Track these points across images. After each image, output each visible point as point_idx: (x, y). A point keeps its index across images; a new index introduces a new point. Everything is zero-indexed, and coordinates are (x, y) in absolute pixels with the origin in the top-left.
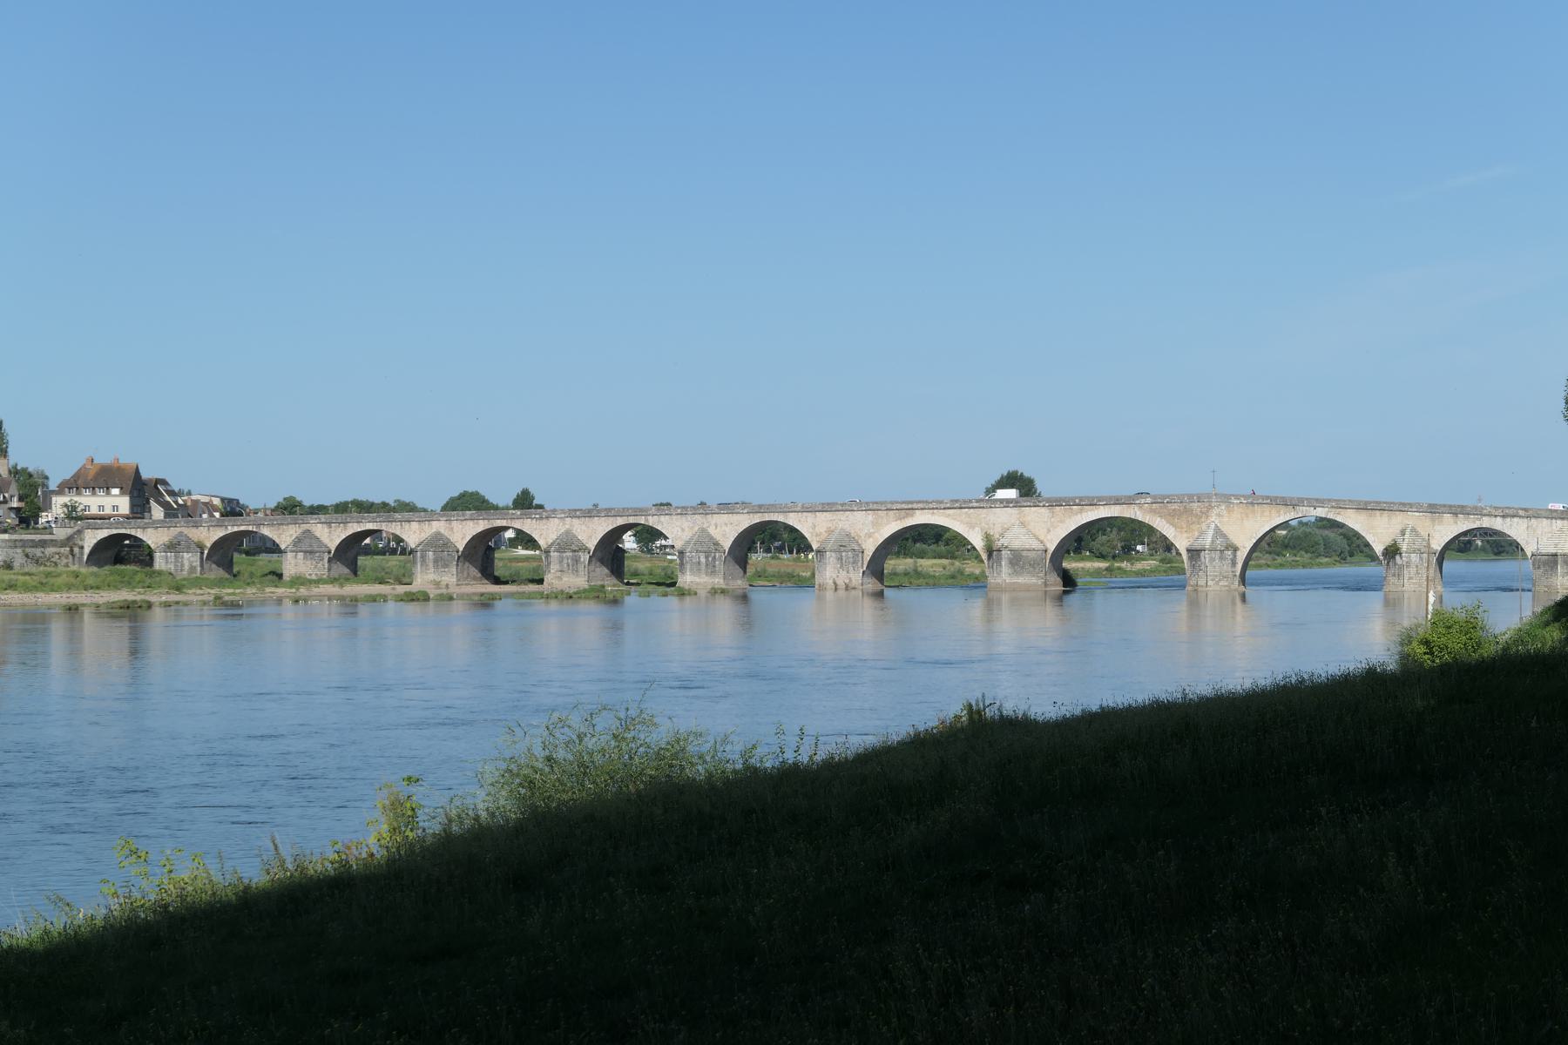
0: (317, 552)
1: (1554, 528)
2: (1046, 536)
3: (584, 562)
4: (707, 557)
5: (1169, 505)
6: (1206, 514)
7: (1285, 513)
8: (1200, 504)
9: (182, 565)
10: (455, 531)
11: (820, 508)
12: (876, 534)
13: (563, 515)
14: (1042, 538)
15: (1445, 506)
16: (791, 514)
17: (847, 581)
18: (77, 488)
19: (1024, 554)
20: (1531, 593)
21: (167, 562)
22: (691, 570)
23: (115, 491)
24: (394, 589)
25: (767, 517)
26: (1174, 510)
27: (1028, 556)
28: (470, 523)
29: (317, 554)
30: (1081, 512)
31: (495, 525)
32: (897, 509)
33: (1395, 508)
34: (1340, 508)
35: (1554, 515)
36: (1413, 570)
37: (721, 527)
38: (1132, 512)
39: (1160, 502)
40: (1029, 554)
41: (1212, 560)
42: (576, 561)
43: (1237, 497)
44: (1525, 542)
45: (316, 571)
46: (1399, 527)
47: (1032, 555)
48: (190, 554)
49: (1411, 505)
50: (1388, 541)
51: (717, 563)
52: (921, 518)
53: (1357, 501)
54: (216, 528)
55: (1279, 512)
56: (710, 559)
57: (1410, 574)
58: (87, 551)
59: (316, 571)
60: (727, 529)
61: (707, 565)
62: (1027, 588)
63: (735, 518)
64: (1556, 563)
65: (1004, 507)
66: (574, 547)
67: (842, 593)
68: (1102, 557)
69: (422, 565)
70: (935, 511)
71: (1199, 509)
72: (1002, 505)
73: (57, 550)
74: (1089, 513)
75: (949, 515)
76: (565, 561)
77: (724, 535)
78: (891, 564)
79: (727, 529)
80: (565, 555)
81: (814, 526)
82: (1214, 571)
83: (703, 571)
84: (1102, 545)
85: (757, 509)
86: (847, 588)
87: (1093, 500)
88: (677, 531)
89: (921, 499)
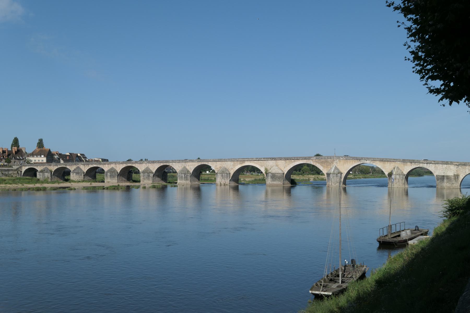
1: (444, 167)
4: (185, 175)
5: (321, 160)
6: (332, 162)
11: (218, 161)
15: (408, 160)
16: (210, 162)
17: (225, 183)
19: (276, 175)
29: (80, 174)
30: (294, 162)
36: (397, 180)
40: (278, 175)
42: (149, 176)
51: (188, 177)
54: (55, 166)
55: (355, 162)
56: (186, 176)
61: (185, 177)
62: (277, 186)
65: (271, 160)
69: (106, 177)
70: (251, 161)
73: (13, 172)
86: (224, 185)
87: (298, 158)
89: (245, 158)
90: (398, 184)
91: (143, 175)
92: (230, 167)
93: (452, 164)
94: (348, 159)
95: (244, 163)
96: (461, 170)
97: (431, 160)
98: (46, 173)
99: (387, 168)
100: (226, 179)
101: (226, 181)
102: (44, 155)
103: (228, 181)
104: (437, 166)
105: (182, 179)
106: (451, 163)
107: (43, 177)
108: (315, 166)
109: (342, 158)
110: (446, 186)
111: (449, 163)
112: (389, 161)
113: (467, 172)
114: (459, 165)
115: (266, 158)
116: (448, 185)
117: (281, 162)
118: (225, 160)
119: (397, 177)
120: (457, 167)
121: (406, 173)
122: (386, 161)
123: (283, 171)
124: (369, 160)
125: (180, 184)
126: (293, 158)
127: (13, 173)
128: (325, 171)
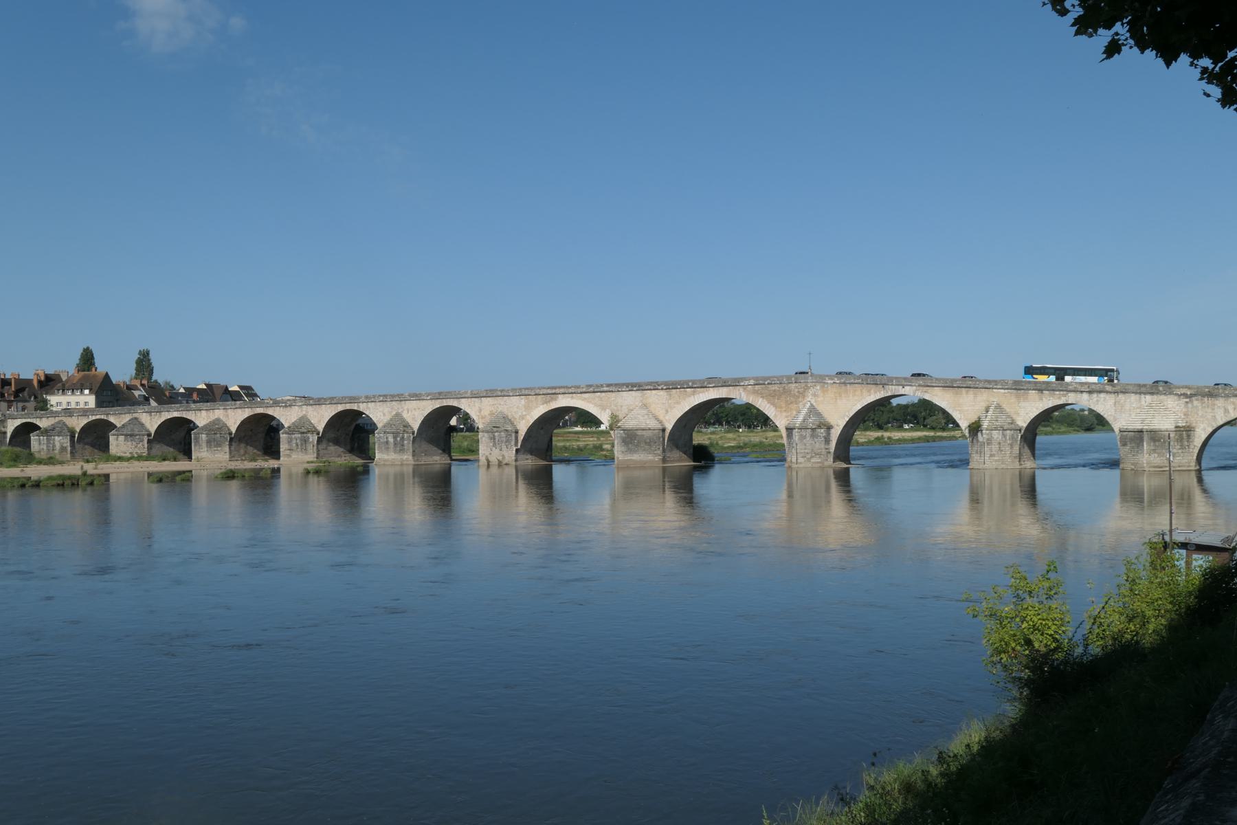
0: (137, 435)
1: (1143, 403)
2: (664, 416)
3: (313, 441)
4: (395, 438)
5: (770, 386)
6: (803, 394)
8: (797, 385)
9: (54, 446)
10: (230, 417)
11: (484, 395)
12: (528, 416)
13: (300, 404)
14: (661, 418)
16: (463, 400)
17: (500, 458)
18: (63, 390)
19: (639, 433)
20: (1116, 473)
21: (40, 444)
22: (380, 448)
23: (87, 392)
24: (96, 468)
25: (348, 407)
26: (774, 391)
27: (643, 435)
28: (239, 411)
29: (138, 437)
30: (694, 393)
31: (256, 412)
32: (543, 394)
33: (981, 385)
34: (928, 386)
35: (1143, 389)
36: (995, 447)
37: (412, 411)
39: (761, 382)
40: (644, 433)
41: (802, 438)
42: (305, 441)
43: (831, 377)
44: (1112, 418)
46: (984, 405)
47: (648, 434)
48: (61, 438)
49: (996, 382)
50: (973, 418)
52: (563, 402)
53: (943, 379)
55: (869, 391)
56: (398, 439)
57: (991, 451)
58: (9, 435)
60: (416, 413)
62: (642, 466)
63: (424, 403)
64: (1142, 440)
65: (630, 390)
66: (303, 430)
67: (494, 470)
68: (933, 428)
69: (195, 445)
71: (796, 390)
72: (627, 389)
74: (701, 394)
75: (585, 399)
76: (294, 441)
77: (413, 419)
78: (860, 436)
79: (416, 413)
80: (293, 436)
81: (480, 410)
82: (805, 449)
83: (392, 449)
84: (933, 422)
85: (437, 396)
86: (500, 464)
88: (379, 414)
89: (562, 385)
91: (289, 438)
93: (1170, 394)
94: (847, 382)
96: (1200, 413)
100: (504, 447)
102: (91, 390)
103: (510, 454)
105: (387, 449)
107: (47, 446)
110: (1148, 463)
112: (972, 386)
114: (1191, 396)
118: (504, 394)
119: (995, 437)
120: (1187, 402)
121: (1025, 423)
122: (962, 387)
123: (657, 419)
125: (382, 463)
126: (690, 384)
128: (781, 422)
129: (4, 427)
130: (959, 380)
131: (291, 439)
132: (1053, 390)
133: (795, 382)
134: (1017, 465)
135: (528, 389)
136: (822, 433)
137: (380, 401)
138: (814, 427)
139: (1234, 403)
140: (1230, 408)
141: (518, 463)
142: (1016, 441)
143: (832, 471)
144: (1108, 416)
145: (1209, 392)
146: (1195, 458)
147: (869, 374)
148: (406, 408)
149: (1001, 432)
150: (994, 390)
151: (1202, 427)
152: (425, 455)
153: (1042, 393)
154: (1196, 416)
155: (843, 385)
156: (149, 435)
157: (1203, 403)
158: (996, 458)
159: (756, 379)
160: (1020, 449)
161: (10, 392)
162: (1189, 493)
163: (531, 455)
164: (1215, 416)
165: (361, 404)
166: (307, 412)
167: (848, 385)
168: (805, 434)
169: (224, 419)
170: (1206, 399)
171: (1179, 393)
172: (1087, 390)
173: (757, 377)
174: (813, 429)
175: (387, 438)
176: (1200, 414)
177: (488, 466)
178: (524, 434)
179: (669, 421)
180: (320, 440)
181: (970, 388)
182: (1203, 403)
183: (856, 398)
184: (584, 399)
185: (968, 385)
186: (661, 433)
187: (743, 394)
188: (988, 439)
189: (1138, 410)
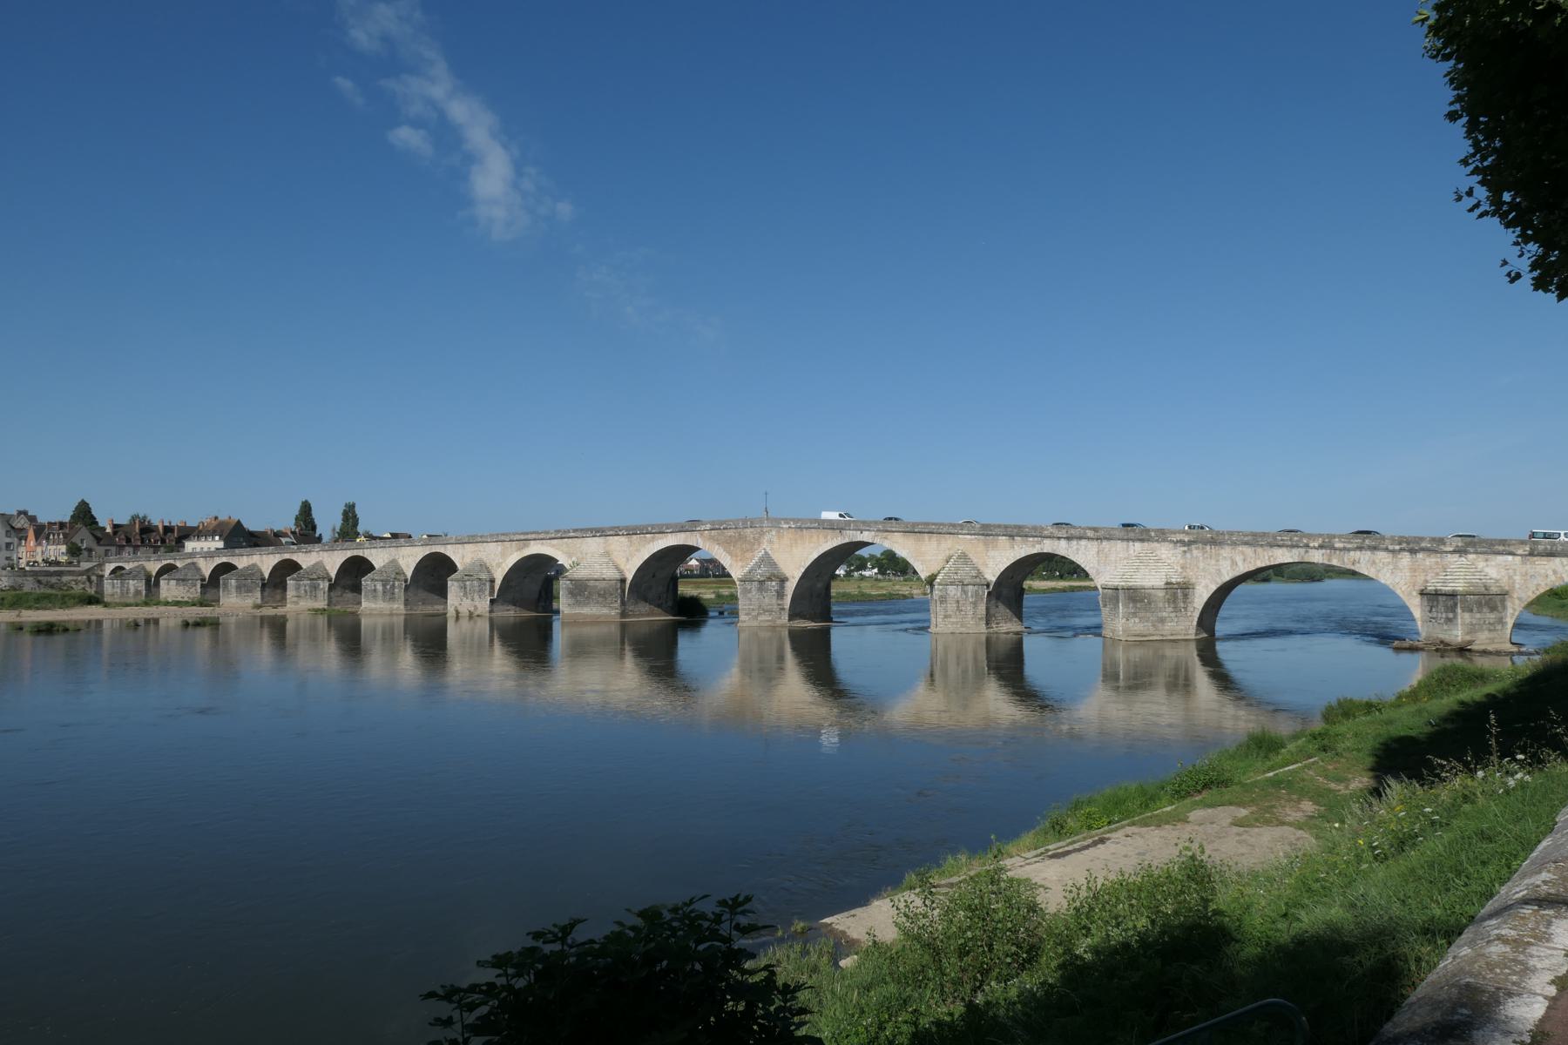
1: (1132, 552)
3: (324, 588)
4: (384, 586)
5: (726, 531)
6: (758, 541)
7: (832, 539)
9: (128, 589)
11: (466, 541)
14: (622, 567)
15: (999, 526)
16: (449, 546)
17: (472, 609)
19: (591, 583)
23: (217, 538)
24: (18, 616)
26: (730, 536)
29: (190, 582)
30: (653, 540)
33: (945, 530)
34: (887, 531)
36: (951, 607)
38: (695, 539)
40: (597, 583)
42: (315, 588)
43: (787, 521)
45: (189, 595)
48: (136, 581)
51: (396, 590)
55: (826, 537)
56: (388, 587)
59: (189, 595)
61: (384, 592)
62: (595, 621)
63: (416, 549)
65: (593, 536)
66: (315, 576)
69: (224, 591)
70: (544, 541)
73: (75, 578)
74: (660, 541)
82: (750, 605)
86: (471, 616)
87: (662, 528)
89: (529, 531)
90: (955, 620)
91: (297, 584)
92: (494, 560)
93: (1164, 540)
94: (803, 526)
95: (527, 546)
96: (1201, 565)
97: (1083, 526)
98: (131, 581)
99: (929, 558)
100: (476, 597)
101: (477, 603)
102: (220, 536)
103: (483, 605)
104: (1106, 550)
105: (375, 597)
106: (1162, 535)
107: (121, 590)
108: (1057, 555)
109: (784, 526)
110: (1124, 631)
111: (1153, 534)
112: (935, 531)
113: (1224, 572)
114: (1190, 543)
115: (582, 530)
116: (1137, 626)
117: (618, 541)
118: (483, 540)
119: (952, 594)
120: (1185, 552)
121: (994, 576)
122: (924, 533)
123: (617, 568)
124: (869, 530)
125: (368, 612)
126: (650, 529)
127: (75, 581)
128: (736, 573)
129: (101, 571)
130: (881, 523)
131: (299, 585)
132: (1026, 536)
133: (751, 527)
134: (983, 628)
135: (503, 535)
136: (773, 587)
137: (381, 547)
138: (762, 579)
139: (1243, 553)
140: (1239, 559)
141: (494, 615)
142: (982, 599)
143: (787, 633)
144: (1090, 568)
145: (1212, 538)
146: (1195, 623)
147: (1062, 524)
148: (401, 554)
149: (960, 587)
150: (960, 536)
151: (1203, 584)
152: (423, 604)
153: (1013, 539)
154: (1196, 570)
155: (799, 530)
156: (203, 580)
157: (1204, 553)
158: (952, 620)
159: (713, 523)
160: (987, 609)
161: (172, 538)
162: (1187, 670)
163: (515, 605)
164: (1219, 570)
165: (365, 550)
166: (323, 558)
167: (804, 530)
168: (749, 587)
169: (259, 564)
170: (1208, 547)
171: (1175, 539)
172: (1064, 536)
173: (713, 521)
174: (762, 582)
175: (375, 586)
176: (1201, 567)
177: (457, 618)
178: (500, 583)
179: (629, 570)
180: (331, 588)
181: (933, 533)
182: (1204, 553)
183: (812, 545)
184: (553, 546)
185: (931, 530)
186: (619, 585)
187: (700, 540)
188: (941, 597)
189: (1125, 561)
